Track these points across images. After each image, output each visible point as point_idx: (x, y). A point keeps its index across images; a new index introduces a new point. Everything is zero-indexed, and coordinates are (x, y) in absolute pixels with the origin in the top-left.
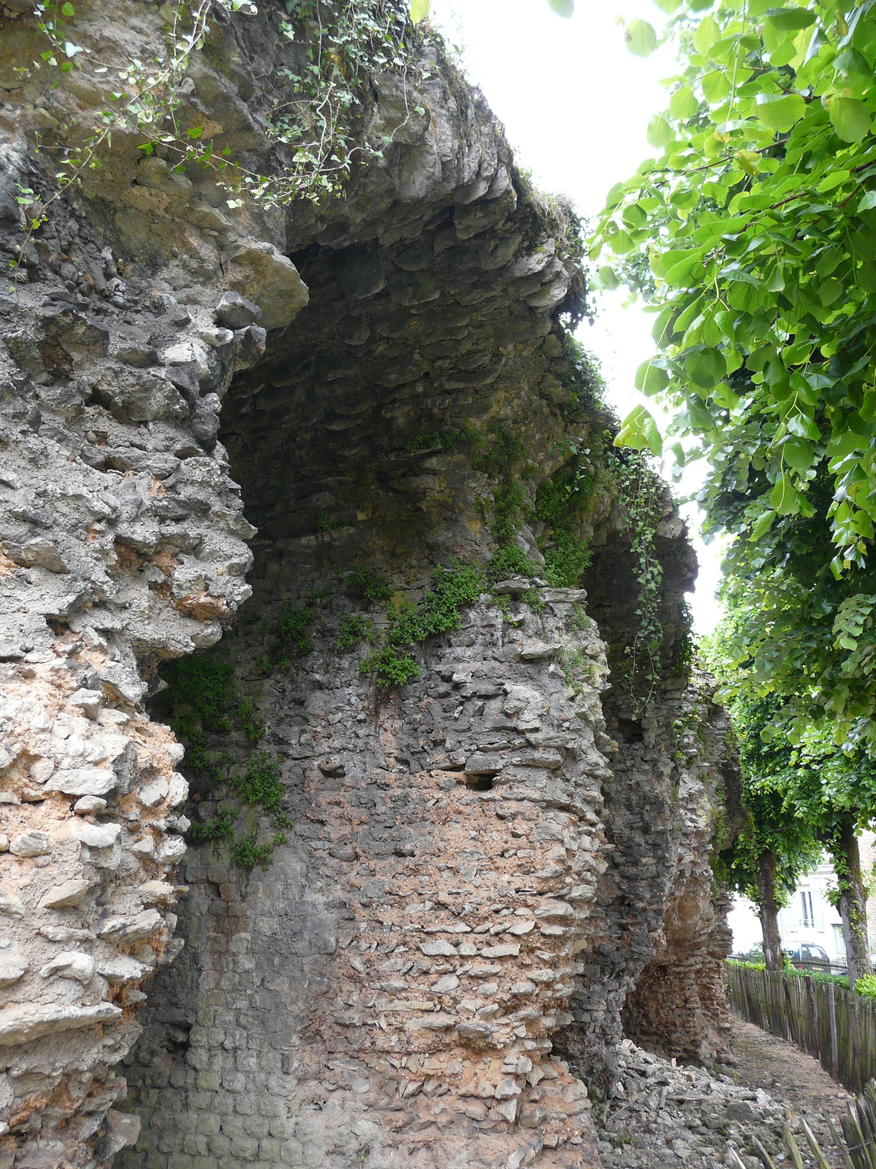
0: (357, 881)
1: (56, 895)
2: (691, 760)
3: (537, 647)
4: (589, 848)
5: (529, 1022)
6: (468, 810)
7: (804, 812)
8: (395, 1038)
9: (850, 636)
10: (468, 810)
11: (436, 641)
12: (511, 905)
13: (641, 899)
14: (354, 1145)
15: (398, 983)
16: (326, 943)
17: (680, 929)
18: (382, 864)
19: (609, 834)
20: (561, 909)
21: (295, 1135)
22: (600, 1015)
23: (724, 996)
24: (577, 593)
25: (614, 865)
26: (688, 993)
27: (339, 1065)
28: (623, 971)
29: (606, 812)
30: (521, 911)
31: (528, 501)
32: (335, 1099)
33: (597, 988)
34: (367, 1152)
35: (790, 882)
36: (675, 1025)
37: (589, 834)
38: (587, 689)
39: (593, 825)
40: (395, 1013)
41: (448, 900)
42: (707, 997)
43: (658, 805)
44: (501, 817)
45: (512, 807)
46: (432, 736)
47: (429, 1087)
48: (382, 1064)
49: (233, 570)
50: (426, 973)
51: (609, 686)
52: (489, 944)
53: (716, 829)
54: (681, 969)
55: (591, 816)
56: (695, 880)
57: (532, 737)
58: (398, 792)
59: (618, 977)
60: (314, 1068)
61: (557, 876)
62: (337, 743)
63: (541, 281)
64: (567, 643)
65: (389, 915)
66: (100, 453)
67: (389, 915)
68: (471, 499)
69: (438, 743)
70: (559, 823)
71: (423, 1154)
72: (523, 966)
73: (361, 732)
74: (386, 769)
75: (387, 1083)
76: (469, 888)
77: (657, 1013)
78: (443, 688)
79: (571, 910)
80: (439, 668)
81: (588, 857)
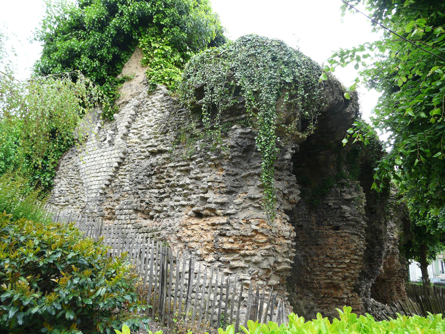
0: (308, 251)
1: (284, 251)
2: (392, 217)
3: (349, 197)
4: (362, 244)
5: (349, 282)
6: (333, 235)
7: (434, 233)
8: (318, 285)
9: (432, 191)
10: (333, 235)
11: (323, 196)
12: (344, 256)
13: (376, 258)
14: (310, 307)
15: (319, 273)
16: (301, 264)
17: (389, 268)
18: (313, 247)
19: (367, 241)
20: (356, 257)
21: (297, 304)
22: (364, 289)
23: (405, 290)
24: (357, 182)
25: (368, 248)
26: (392, 288)
27: (305, 290)
28: (371, 277)
29: (366, 235)
30: (346, 258)
31: (345, 159)
32: (305, 298)
33: (363, 282)
34: (313, 308)
35: (433, 256)
36: (388, 297)
37: (362, 240)
38: (361, 206)
39: (363, 238)
40: (318, 279)
41: (330, 255)
42: (399, 290)
43: (381, 232)
44: (341, 237)
45: (344, 234)
46: (324, 218)
47: (326, 296)
48: (315, 291)
49: (298, 195)
50: (325, 271)
51: (366, 205)
52: (339, 265)
53: (400, 238)
54: (390, 281)
55: (362, 236)
56: (393, 254)
57: (348, 218)
58: (316, 231)
59: (369, 279)
60: (300, 291)
61: (355, 250)
62: (301, 219)
63: (349, 114)
64: (355, 195)
65: (315, 258)
66: (277, 177)
67: (315, 258)
68: (331, 160)
69: (326, 220)
70: (355, 238)
71: (325, 309)
72: (347, 270)
73: (306, 217)
74: (313, 225)
75: (317, 295)
76: (334, 252)
77: (382, 294)
78: (326, 207)
79: (358, 258)
80: (325, 202)
81: (362, 246)
